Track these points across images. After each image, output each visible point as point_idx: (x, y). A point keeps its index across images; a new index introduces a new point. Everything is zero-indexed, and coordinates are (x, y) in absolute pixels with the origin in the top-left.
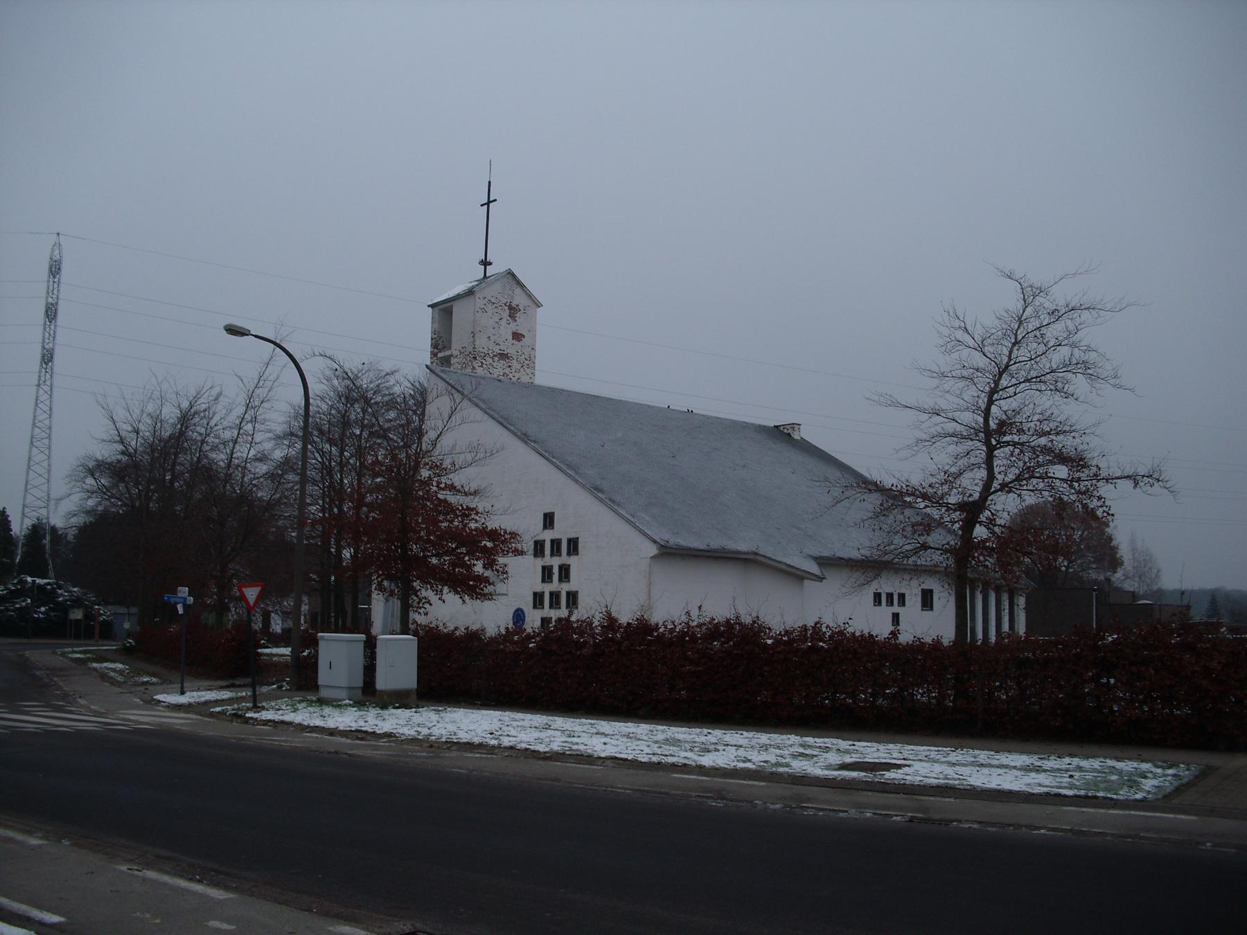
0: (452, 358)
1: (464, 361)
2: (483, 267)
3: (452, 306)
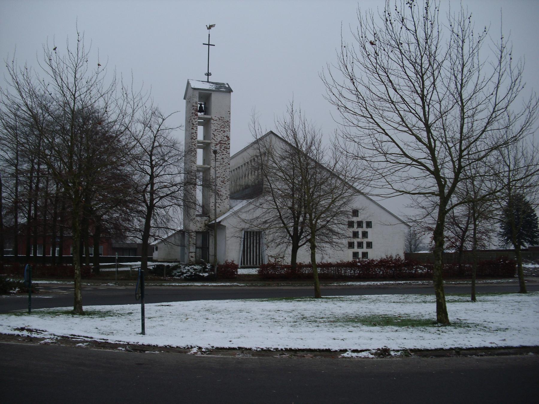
0: (212, 121)
1: (223, 124)
2: (209, 72)
3: (211, 93)
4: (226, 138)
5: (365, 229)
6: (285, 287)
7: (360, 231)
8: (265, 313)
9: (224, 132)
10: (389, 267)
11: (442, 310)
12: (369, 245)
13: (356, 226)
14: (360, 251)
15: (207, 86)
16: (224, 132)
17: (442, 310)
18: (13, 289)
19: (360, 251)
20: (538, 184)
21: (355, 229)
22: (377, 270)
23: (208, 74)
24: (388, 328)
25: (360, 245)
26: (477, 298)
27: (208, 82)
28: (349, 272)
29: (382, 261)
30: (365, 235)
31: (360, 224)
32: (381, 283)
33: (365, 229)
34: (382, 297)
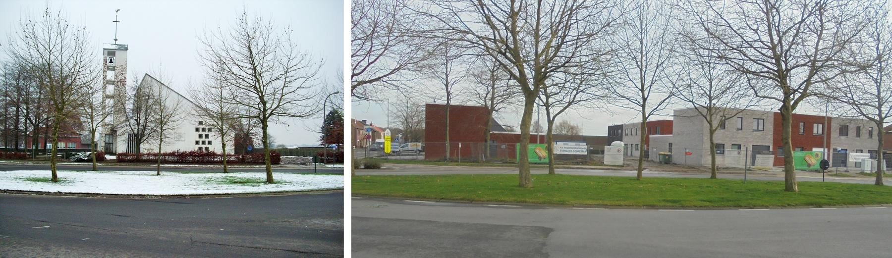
4: (124, 78)
5: (207, 132)
6: (132, 166)
7: (204, 134)
8: (844, 192)
9: (123, 74)
10: (195, 156)
11: (54, 175)
12: (210, 143)
13: (207, 131)
14: (204, 147)
15: (114, 47)
16: (123, 74)
17: (54, 175)
18: (33, 88)
19: (204, 147)
20: (754, 10)
21: (201, 132)
22: (188, 158)
23: (116, 40)
24: (252, 192)
25: (203, 143)
26: (160, 173)
27: (116, 44)
28: (171, 159)
29: (190, 153)
30: (200, 136)
31: (204, 130)
32: (183, 165)
33: (207, 132)
34: (124, 172)
